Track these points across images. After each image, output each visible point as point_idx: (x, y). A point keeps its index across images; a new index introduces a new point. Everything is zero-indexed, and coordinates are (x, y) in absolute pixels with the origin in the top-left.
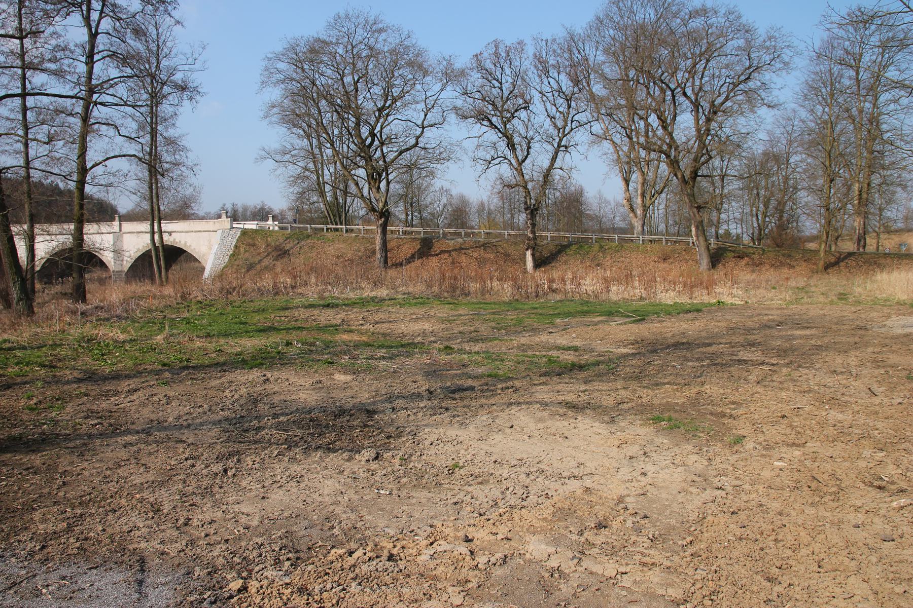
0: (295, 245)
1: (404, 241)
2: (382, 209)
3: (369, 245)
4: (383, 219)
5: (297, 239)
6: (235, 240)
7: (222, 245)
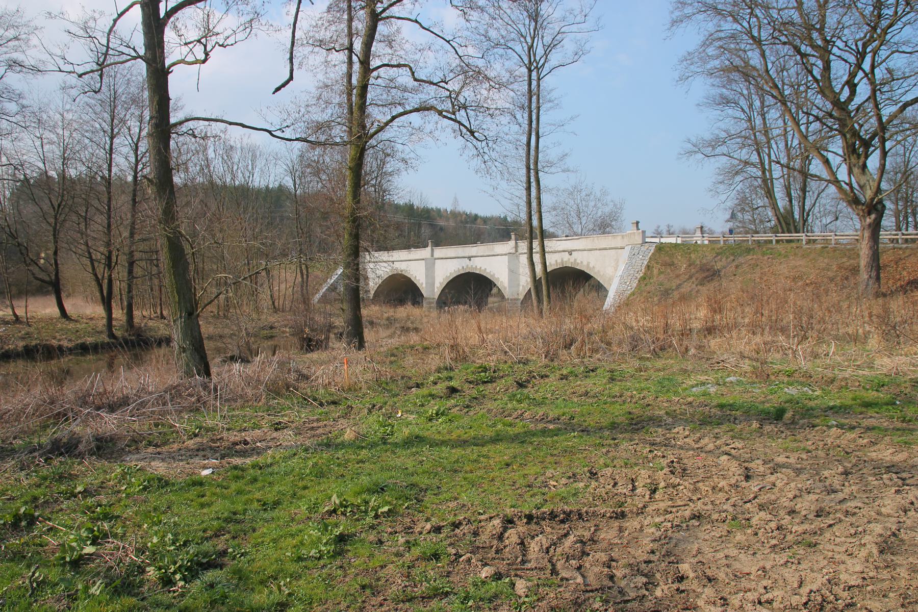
0: (730, 263)
1: (908, 252)
2: (872, 199)
3: (845, 260)
4: (873, 216)
5: (733, 254)
6: (647, 258)
7: (630, 265)
